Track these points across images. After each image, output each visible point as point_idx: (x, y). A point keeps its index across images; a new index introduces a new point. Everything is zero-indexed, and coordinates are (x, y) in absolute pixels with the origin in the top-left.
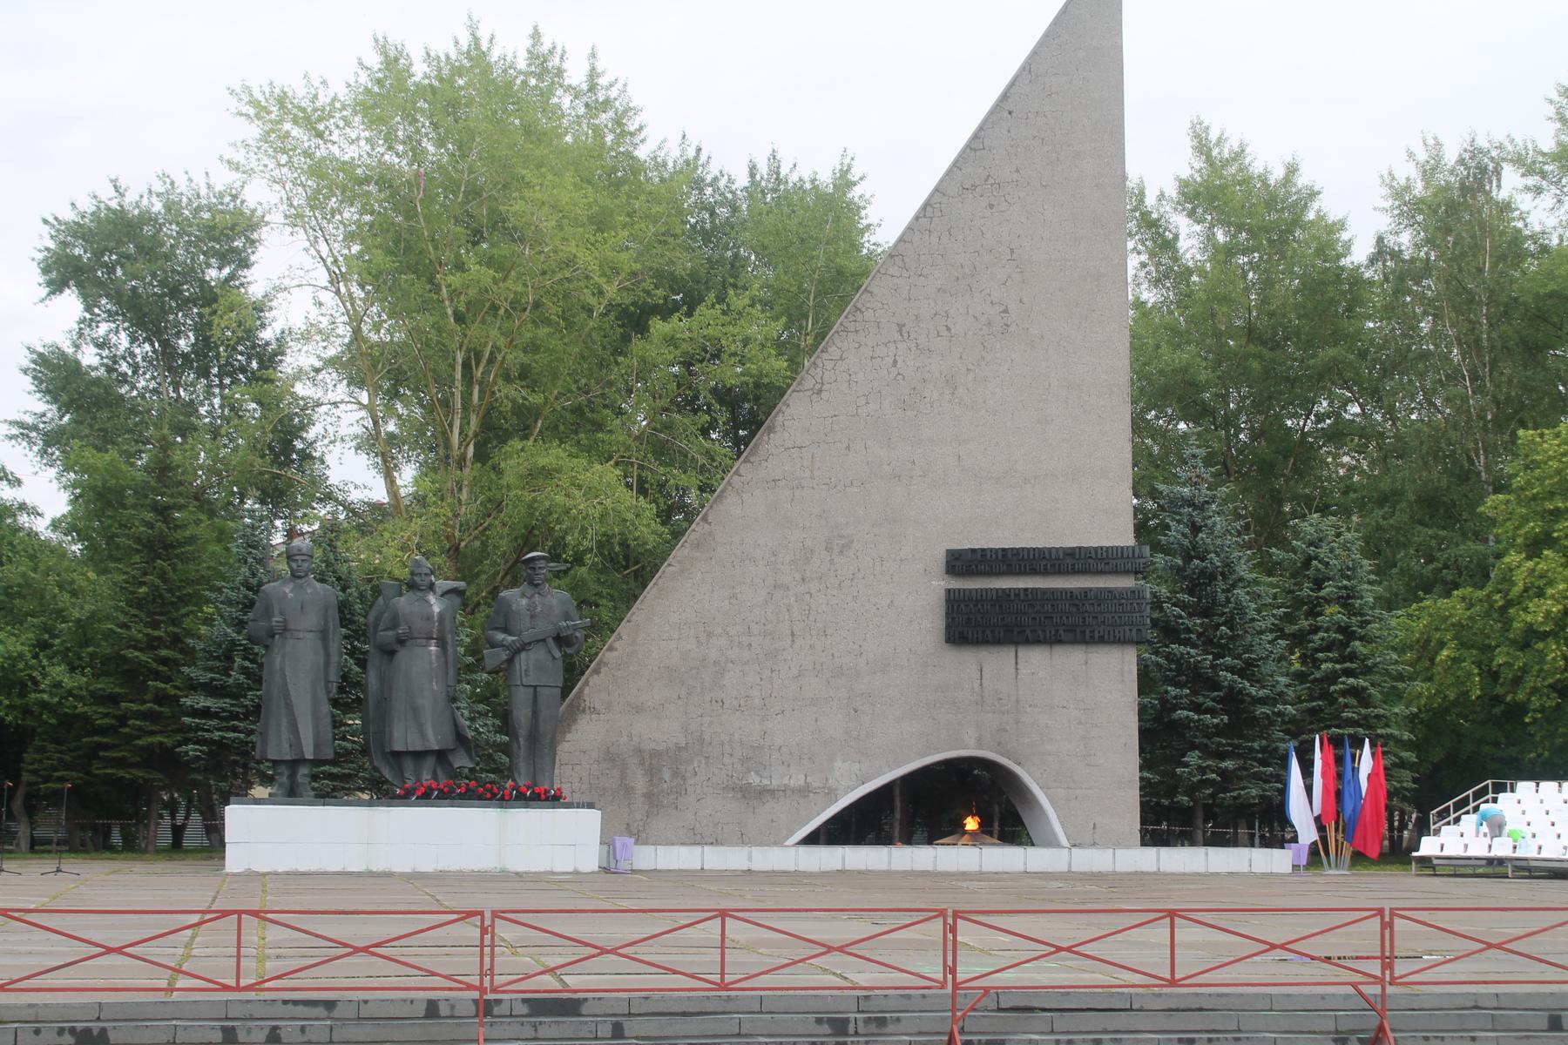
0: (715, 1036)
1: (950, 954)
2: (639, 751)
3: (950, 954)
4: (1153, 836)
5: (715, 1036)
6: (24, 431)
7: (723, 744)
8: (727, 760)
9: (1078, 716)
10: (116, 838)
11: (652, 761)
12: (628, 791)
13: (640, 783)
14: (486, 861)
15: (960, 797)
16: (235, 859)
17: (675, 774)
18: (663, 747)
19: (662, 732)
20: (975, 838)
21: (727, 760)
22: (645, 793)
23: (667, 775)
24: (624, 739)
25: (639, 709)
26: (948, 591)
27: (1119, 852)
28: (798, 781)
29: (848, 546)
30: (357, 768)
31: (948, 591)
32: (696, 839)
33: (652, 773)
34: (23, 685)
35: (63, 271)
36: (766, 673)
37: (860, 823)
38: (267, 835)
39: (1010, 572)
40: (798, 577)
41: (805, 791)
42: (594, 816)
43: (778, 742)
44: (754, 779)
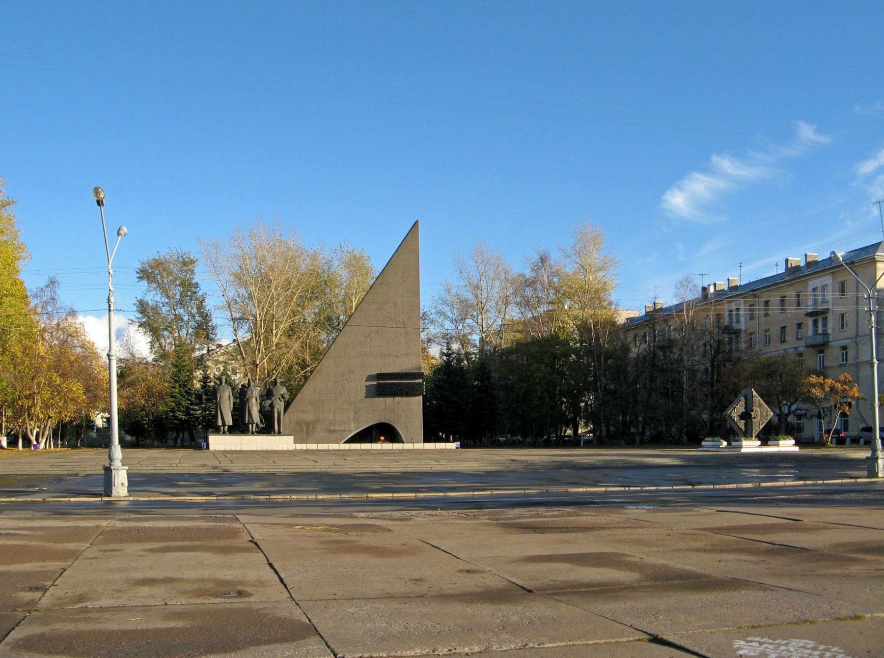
1: (861, 496)
3: (861, 496)
4: (427, 439)
6: (863, 260)
9: (409, 412)
10: (170, 442)
11: (308, 424)
12: (302, 431)
13: (305, 429)
14: (265, 447)
16: (212, 448)
19: (309, 417)
20: (384, 441)
25: (303, 411)
28: (342, 428)
30: (240, 427)
32: (318, 442)
33: (308, 427)
35: (197, 283)
37: (352, 440)
38: (218, 442)
39: (392, 379)
41: (344, 431)
44: (332, 428)
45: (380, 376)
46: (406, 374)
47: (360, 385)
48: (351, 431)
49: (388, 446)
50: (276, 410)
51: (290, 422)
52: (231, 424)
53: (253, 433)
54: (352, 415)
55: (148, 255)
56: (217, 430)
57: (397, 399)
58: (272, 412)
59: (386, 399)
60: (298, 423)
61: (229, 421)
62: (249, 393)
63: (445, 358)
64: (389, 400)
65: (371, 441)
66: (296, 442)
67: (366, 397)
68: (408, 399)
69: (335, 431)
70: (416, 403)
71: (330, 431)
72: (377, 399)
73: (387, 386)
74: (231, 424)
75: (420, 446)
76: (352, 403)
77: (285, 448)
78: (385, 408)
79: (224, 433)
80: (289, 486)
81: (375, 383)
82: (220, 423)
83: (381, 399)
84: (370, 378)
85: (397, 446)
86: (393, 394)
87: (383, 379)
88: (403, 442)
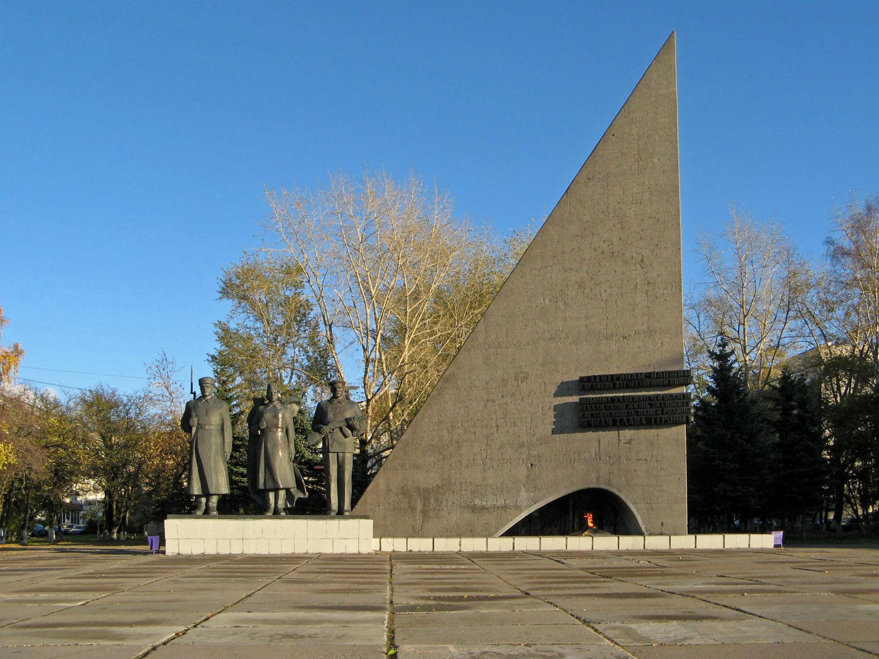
0: (71, 551)
2: (418, 489)
5: (71, 551)
7: (461, 484)
8: (463, 493)
9: (655, 464)
11: (425, 494)
12: (413, 509)
15: (600, 509)
16: (171, 548)
17: (437, 500)
18: (430, 486)
19: (428, 479)
21: (463, 493)
22: (418, 510)
23: (432, 501)
24: (410, 483)
25: (417, 467)
26: (556, 408)
27: (699, 537)
28: (501, 502)
29: (527, 378)
31: (556, 408)
33: (425, 499)
34: (443, 252)
36: (484, 447)
37: (530, 526)
38: (184, 535)
40: (500, 395)
41: (505, 507)
42: (369, 523)
43: (491, 482)
44: (477, 502)
45: (587, 384)
46: (649, 375)
47: (542, 404)
48: (519, 509)
49: (606, 543)
50: (332, 457)
51: (389, 490)
52: (225, 490)
53: (276, 513)
54: (522, 472)
55: (231, 261)
56: (184, 505)
57: (627, 434)
58: (326, 461)
59: (601, 434)
60: (405, 492)
61: (221, 485)
62: (268, 416)
63: (716, 364)
64: (608, 436)
65: (564, 532)
66: (380, 532)
67: (554, 432)
68: (651, 433)
69: (484, 508)
70: (671, 444)
71: (474, 509)
72: (579, 436)
73: (604, 404)
74: (225, 490)
75: (685, 542)
76: (522, 445)
77: (352, 548)
78: (598, 455)
79: (207, 513)
80: (457, 590)
81: (575, 399)
82: (196, 489)
83: (590, 435)
84: (564, 389)
85: (628, 542)
86: (617, 424)
87: (593, 389)
88: (637, 531)
